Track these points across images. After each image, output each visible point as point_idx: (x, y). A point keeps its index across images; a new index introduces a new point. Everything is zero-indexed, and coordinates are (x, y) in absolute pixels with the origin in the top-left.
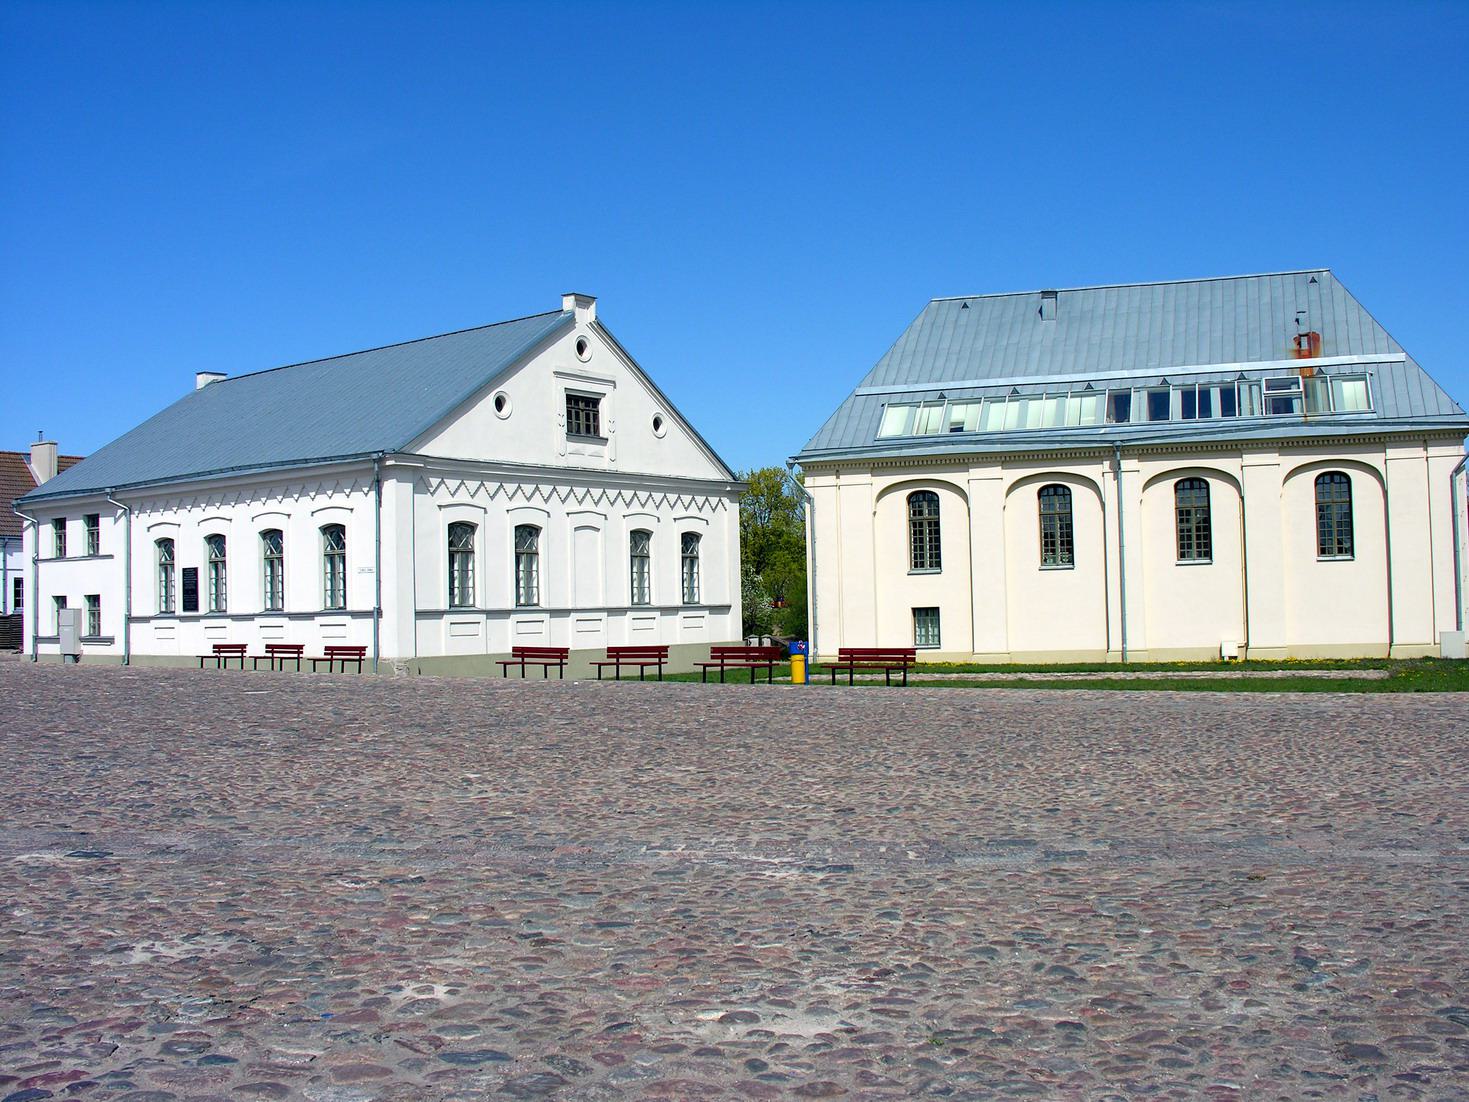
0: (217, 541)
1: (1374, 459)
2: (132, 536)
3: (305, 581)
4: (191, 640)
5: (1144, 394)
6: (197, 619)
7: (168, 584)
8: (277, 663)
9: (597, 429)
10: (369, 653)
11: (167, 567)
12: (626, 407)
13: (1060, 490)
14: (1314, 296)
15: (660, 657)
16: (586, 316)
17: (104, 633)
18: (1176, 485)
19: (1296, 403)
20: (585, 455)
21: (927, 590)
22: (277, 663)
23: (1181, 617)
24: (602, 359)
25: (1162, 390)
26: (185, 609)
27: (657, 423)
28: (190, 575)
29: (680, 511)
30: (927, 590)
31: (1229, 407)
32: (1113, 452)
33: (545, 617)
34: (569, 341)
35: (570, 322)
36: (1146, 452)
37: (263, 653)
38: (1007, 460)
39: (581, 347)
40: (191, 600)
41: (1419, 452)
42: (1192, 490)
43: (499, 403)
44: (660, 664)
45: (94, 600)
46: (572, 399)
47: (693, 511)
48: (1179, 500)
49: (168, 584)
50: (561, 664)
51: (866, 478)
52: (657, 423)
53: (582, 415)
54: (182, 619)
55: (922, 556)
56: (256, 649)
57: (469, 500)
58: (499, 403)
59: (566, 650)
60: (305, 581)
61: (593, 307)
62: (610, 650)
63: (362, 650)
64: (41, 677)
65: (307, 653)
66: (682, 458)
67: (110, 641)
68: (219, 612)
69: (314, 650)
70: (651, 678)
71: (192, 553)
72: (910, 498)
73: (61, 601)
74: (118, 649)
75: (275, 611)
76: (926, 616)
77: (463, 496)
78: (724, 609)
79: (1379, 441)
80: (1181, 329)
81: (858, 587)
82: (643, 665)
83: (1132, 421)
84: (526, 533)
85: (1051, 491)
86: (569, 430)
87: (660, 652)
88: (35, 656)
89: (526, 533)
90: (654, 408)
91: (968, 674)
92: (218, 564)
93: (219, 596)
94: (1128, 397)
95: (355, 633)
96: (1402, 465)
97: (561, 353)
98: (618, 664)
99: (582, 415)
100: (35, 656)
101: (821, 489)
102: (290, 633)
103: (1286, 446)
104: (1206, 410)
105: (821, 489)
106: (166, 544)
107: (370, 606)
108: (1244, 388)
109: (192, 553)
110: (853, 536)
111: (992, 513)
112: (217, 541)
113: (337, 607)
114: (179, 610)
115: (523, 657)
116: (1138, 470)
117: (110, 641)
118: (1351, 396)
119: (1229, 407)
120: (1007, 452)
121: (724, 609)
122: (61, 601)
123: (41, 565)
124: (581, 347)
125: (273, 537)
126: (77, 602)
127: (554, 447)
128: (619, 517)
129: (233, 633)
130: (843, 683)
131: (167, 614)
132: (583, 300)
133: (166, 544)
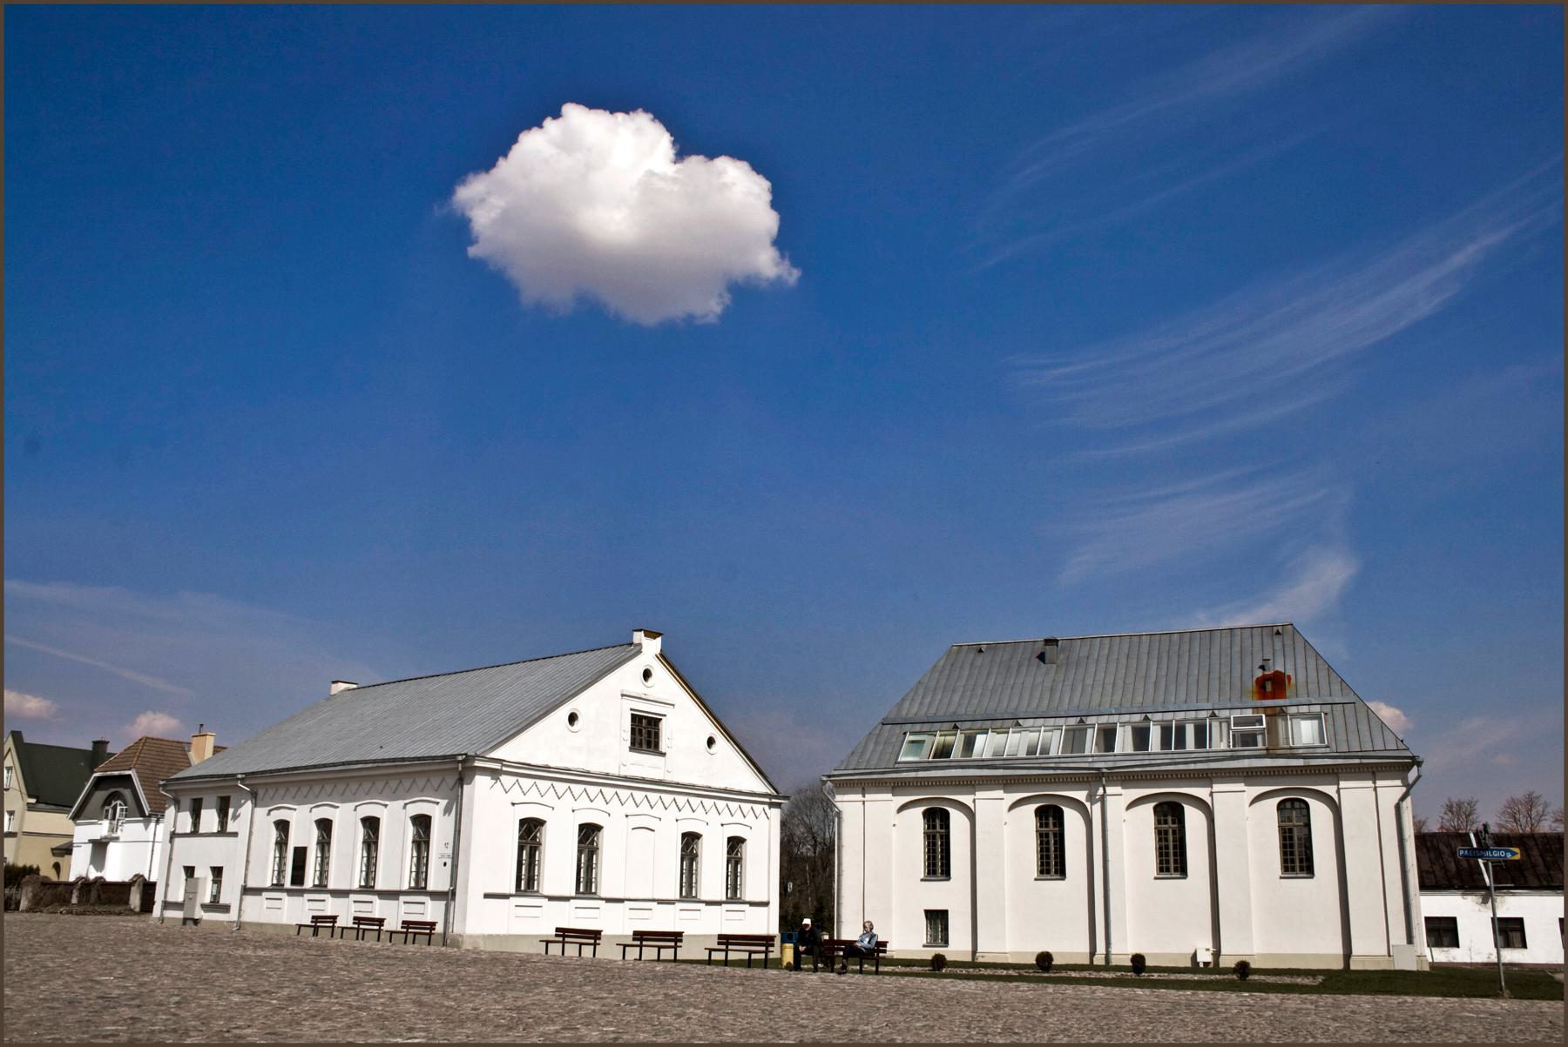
0: (325, 826)
1: (966, 799)
2: (254, 820)
3: (395, 867)
4: (294, 911)
5: (1129, 729)
6: (301, 893)
7: (282, 858)
8: (410, 937)
9: (657, 745)
10: (439, 929)
11: (282, 844)
12: (685, 723)
13: (1297, 805)
14: (1278, 645)
15: (676, 941)
16: (652, 647)
17: (222, 901)
18: (1279, 804)
19: (1259, 738)
20: (644, 765)
21: (939, 895)
22: (410, 937)
23: (1157, 921)
24: (665, 685)
25: (1144, 725)
26: (293, 883)
27: (711, 742)
28: (301, 853)
29: (726, 818)
30: (939, 895)
31: (1201, 740)
32: (1095, 779)
33: (544, 902)
34: (634, 667)
35: (638, 650)
36: (1127, 778)
37: (350, 924)
38: (1007, 783)
39: (647, 674)
40: (298, 877)
41: (859, 797)
42: (1170, 814)
43: (573, 718)
44: (675, 947)
45: (217, 872)
46: (636, 719)
47: (738, 817)
48: (1282, 819)
49: (282, 858)
50: (595, 945)
51: (999, 793)
52: (711, 742)
53: (645, 733)
54: (290, 892)
55: (1168, 862)
56: (345, 921)
57: (538, 799)
58: (573, 718)
59: (680, 934)
60: (395, 867)
61: (659, 640)
62: (720, 937)
63: (432, 925)
64: (167, 937)
65: (340, 923)
66: (739, 774)
67: (226, 909)
68: (321, 888)
69: (392, 924)
70: (717, 963)
71: (303, 834)
72: (1281, 806)
73: (190, 871)
74: (232, 916)
75: (368, 888)
76: (937, 919)
77: (533, 796)
78: (766, 904)
79: (1334, 773)
80: (1163, 672)
81: (882, 885)
82: (660, 948)
83: (1116, 751)
84: (589, 833)
85: (1288, 805)
86: (633, 743)
87: (676, 937)
88: (162, 919)
89: (589, 833)
90: (711, 729)
91: (974, 969)
92: (324, 844)
93: (323, 873)
94: (1115, 730)
95: (431, 911)
96: (1355, 795)
97: (627, 676)
98: (641, 946)
99: (645, 733)
100: (162, 919)
101: (848, 805)
102: (378, 908)
103: (1249, 776)
104: (1181, 742)
105: (848, 805)
106: (283, 826)
107: (445, 887)
108: (1215, 724)
109: (303, 834)
110: (877, 840)
111: (1001, 827)
112: (325, 826)
113: (419, 888)
114: (288, 884)
115: (727, 944)
116: (1118, 797)
117: (226, 909)
118: (1305, 732)
119: (1201, 740)
120: (1004, 776)
121: (766, 904)
122: (190, 871)
123: (177, 840)
124: (647, 674)
125: (371, 824)
126: (204, 874)
127: (618, 756)
128: (672, 820)
129: (330, 906)
130: (869, 973)
131: (278, 887)
132: (651, 634)
133: (283, 826)
